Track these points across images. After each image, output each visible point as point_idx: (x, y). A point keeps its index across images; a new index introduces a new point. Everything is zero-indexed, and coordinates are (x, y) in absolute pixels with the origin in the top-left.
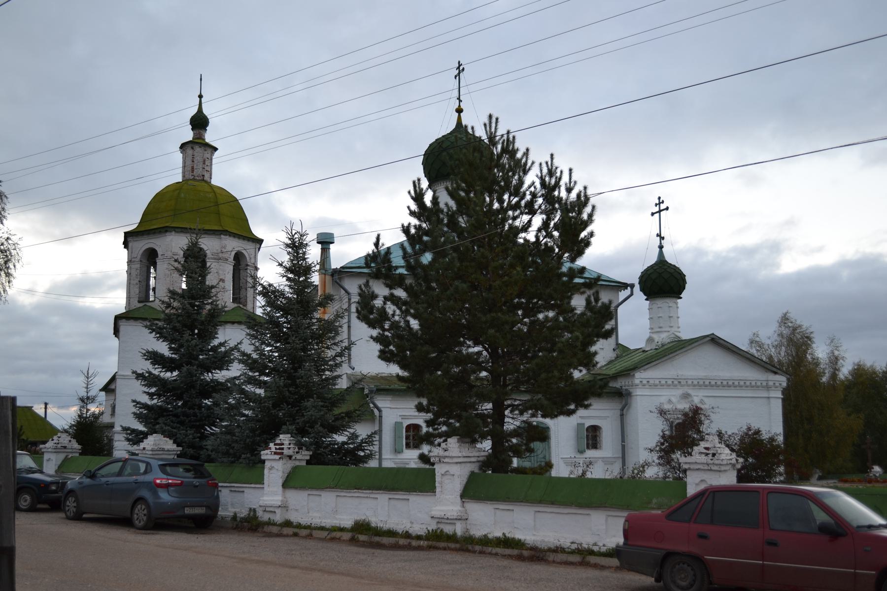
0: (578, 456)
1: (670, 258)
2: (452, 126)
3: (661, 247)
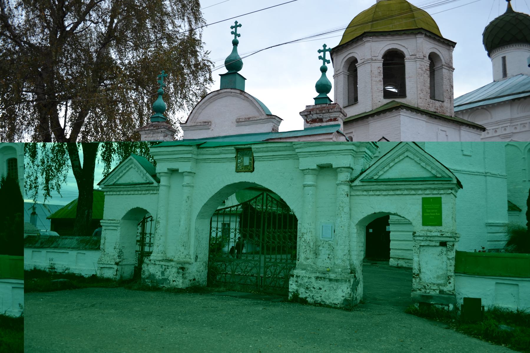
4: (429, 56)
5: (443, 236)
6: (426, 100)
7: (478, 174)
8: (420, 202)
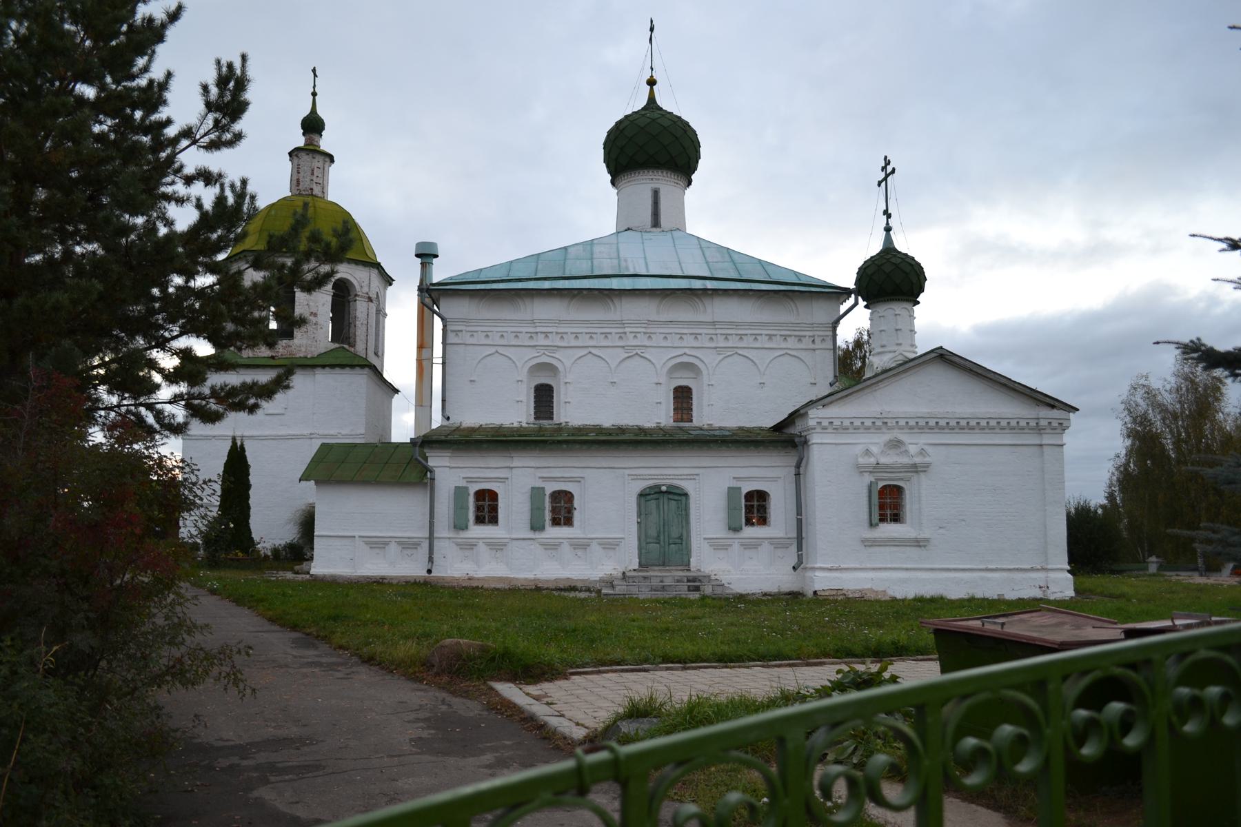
0: (731, 535)
1: (666, 102)
3: (888, 229)
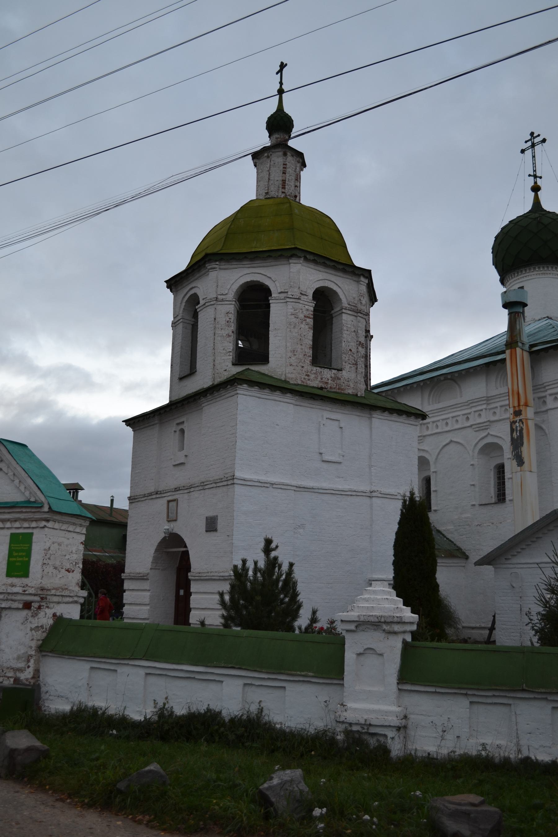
2: (528, 207)
4: (315, 293)
5: (26, 592)
6: (303, 367)
7: (354, 493)
8: (8, 539)
